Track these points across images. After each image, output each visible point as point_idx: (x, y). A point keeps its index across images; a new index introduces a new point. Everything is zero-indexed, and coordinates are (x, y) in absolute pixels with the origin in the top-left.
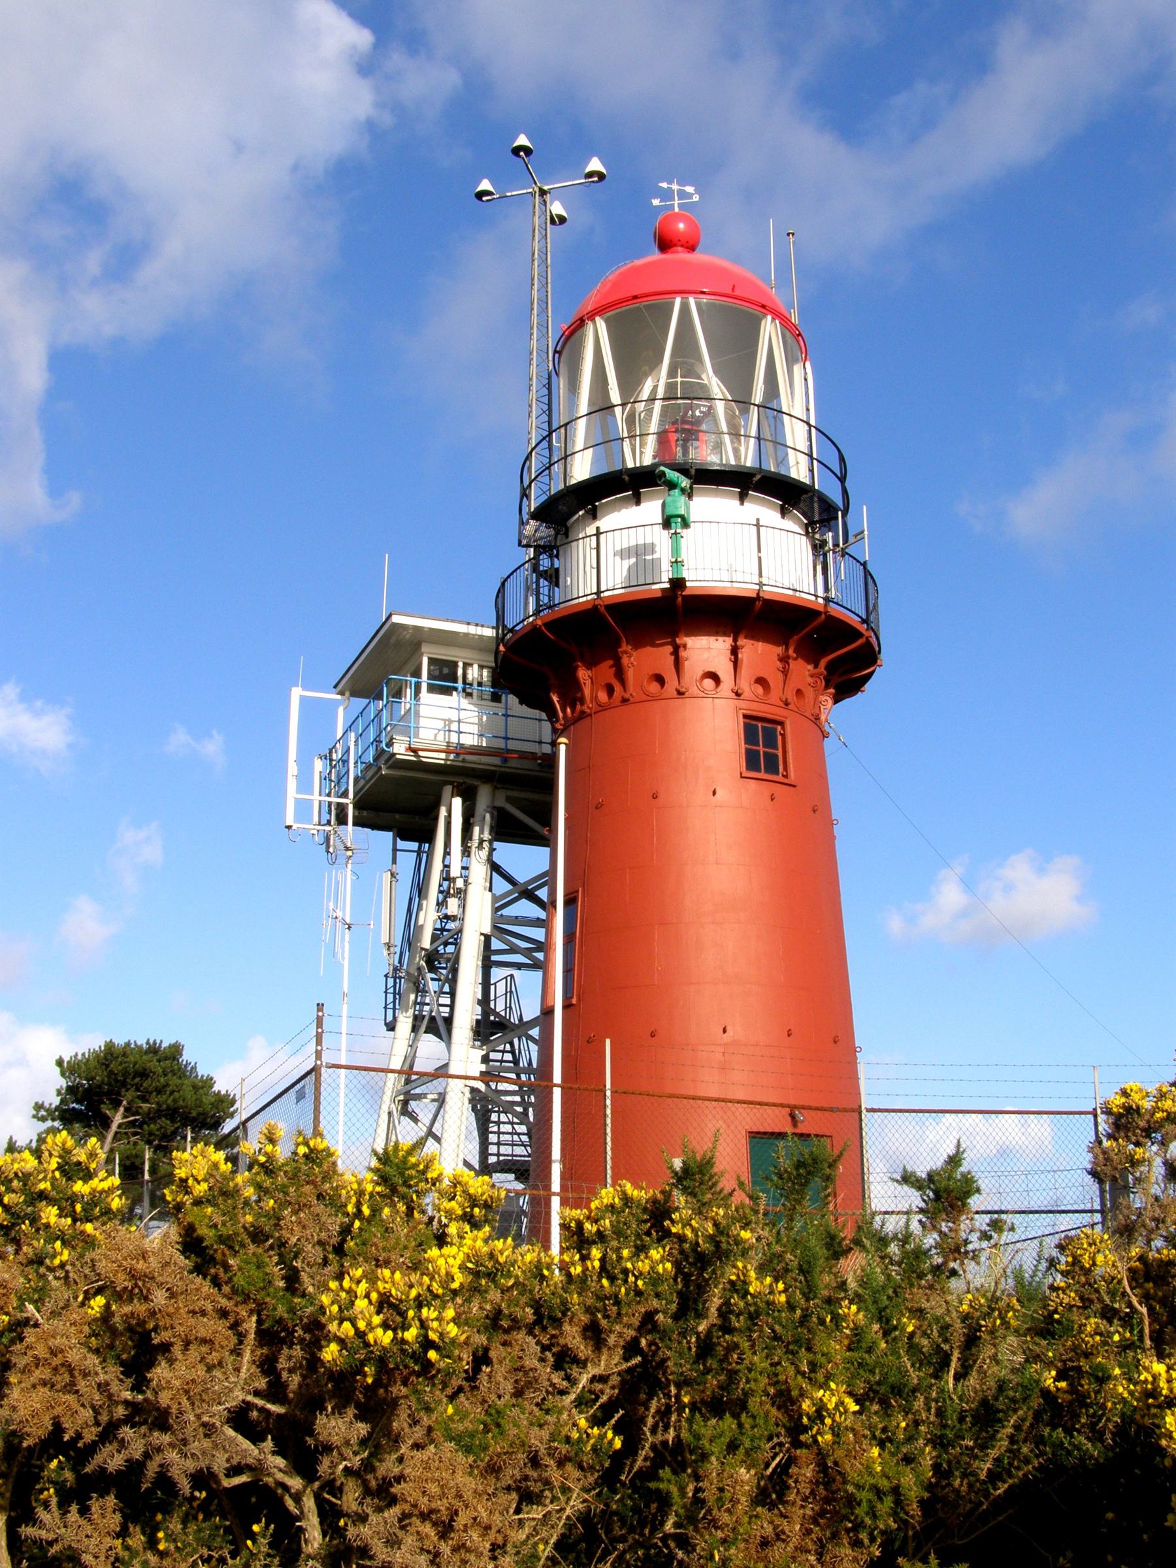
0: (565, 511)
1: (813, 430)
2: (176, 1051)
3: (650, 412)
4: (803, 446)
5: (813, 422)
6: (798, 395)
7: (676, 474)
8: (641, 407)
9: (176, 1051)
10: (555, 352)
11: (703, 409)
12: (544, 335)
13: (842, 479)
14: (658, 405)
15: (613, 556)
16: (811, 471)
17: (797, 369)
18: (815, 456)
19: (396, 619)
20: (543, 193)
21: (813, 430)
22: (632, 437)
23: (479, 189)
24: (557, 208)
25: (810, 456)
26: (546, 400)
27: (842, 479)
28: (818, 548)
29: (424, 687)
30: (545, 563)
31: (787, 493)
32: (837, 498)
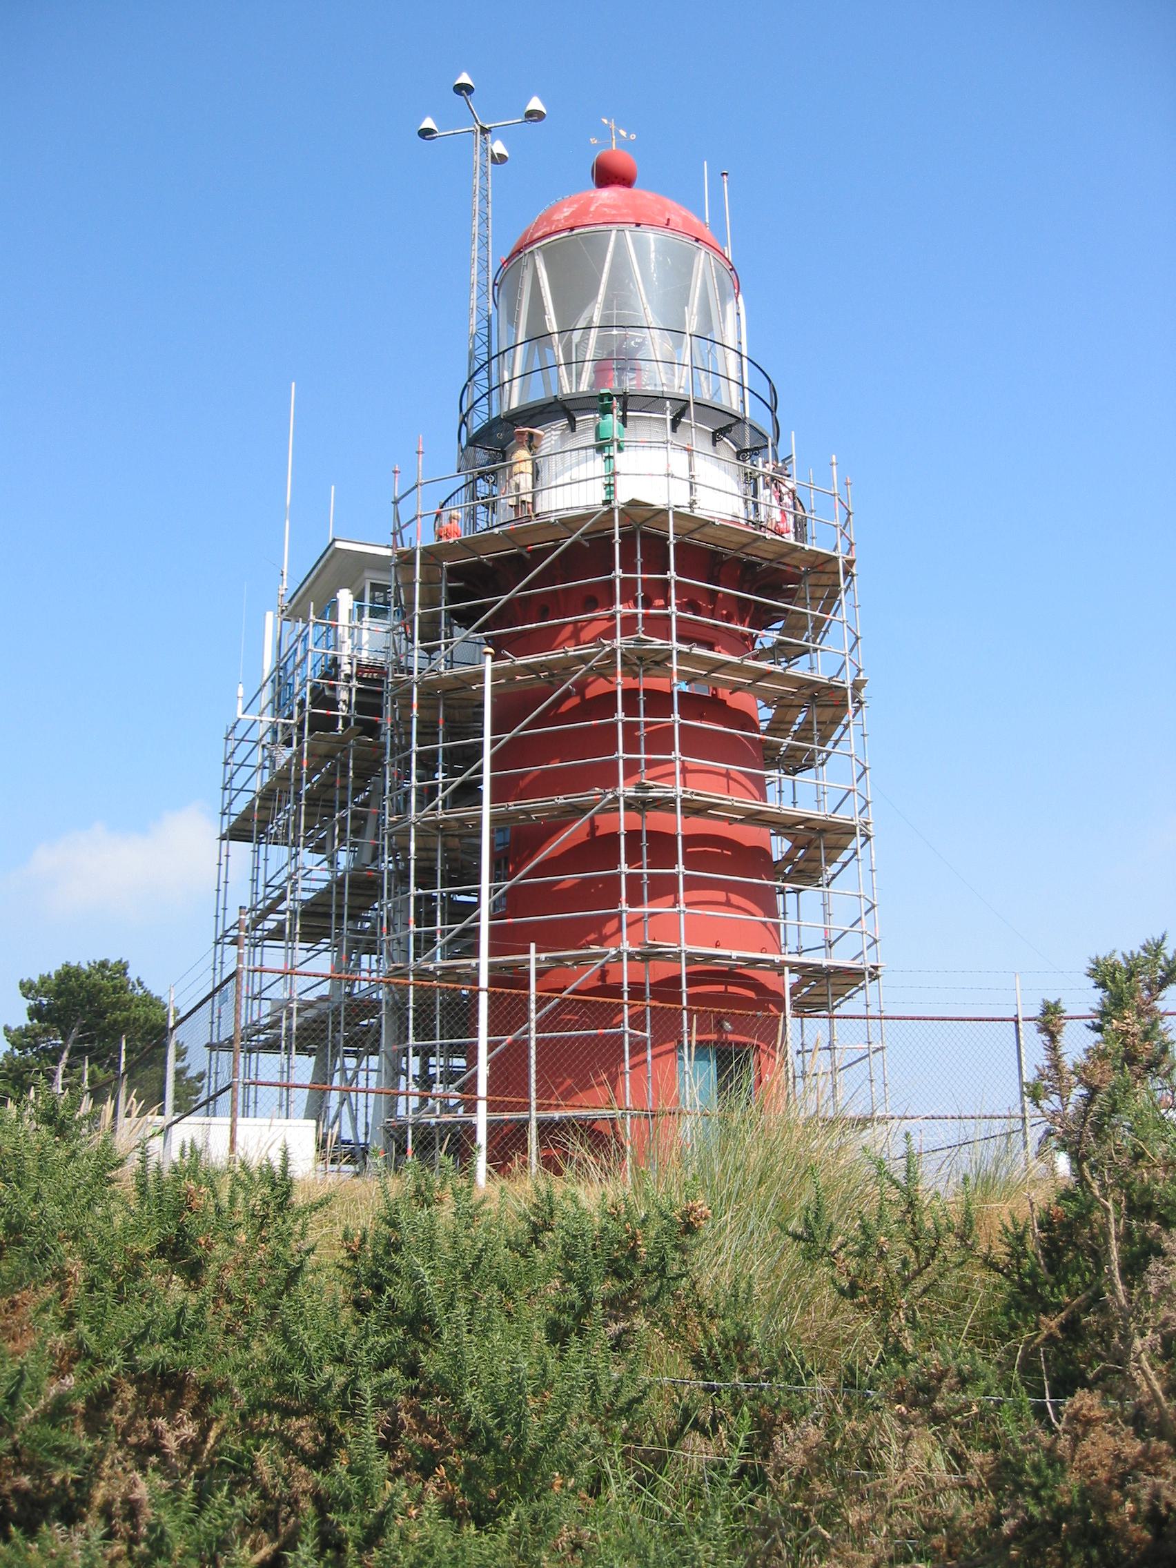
0: (496, 440)
1: (745, 360)
2: (122, 968)
3: (585, 340)
4: (733, 374)
5: (744, 353)
6: (733, 325)
7: (606, 405)
8: (577, 336)
9: (122, 968)
10: (495, 284)
11: (638, 341)
12: (484, 269)
13: (773, 410)
14: (594, 333)
15: (568, 483)
16: (743, 402)
17: (730, 308)
18: (746, 385)
19: (338, 545)
20: (484, 131)
21: (745, 360)
22: (568, 364)
23: (423, 126)
24: (498, 148)
25: (741, 385)
26: (485, 331)
27: (773, 410)
28: (750, 479)
29: (367, 611)
30: (483, 487)
31: (725, 427)
32: (767, 428)
